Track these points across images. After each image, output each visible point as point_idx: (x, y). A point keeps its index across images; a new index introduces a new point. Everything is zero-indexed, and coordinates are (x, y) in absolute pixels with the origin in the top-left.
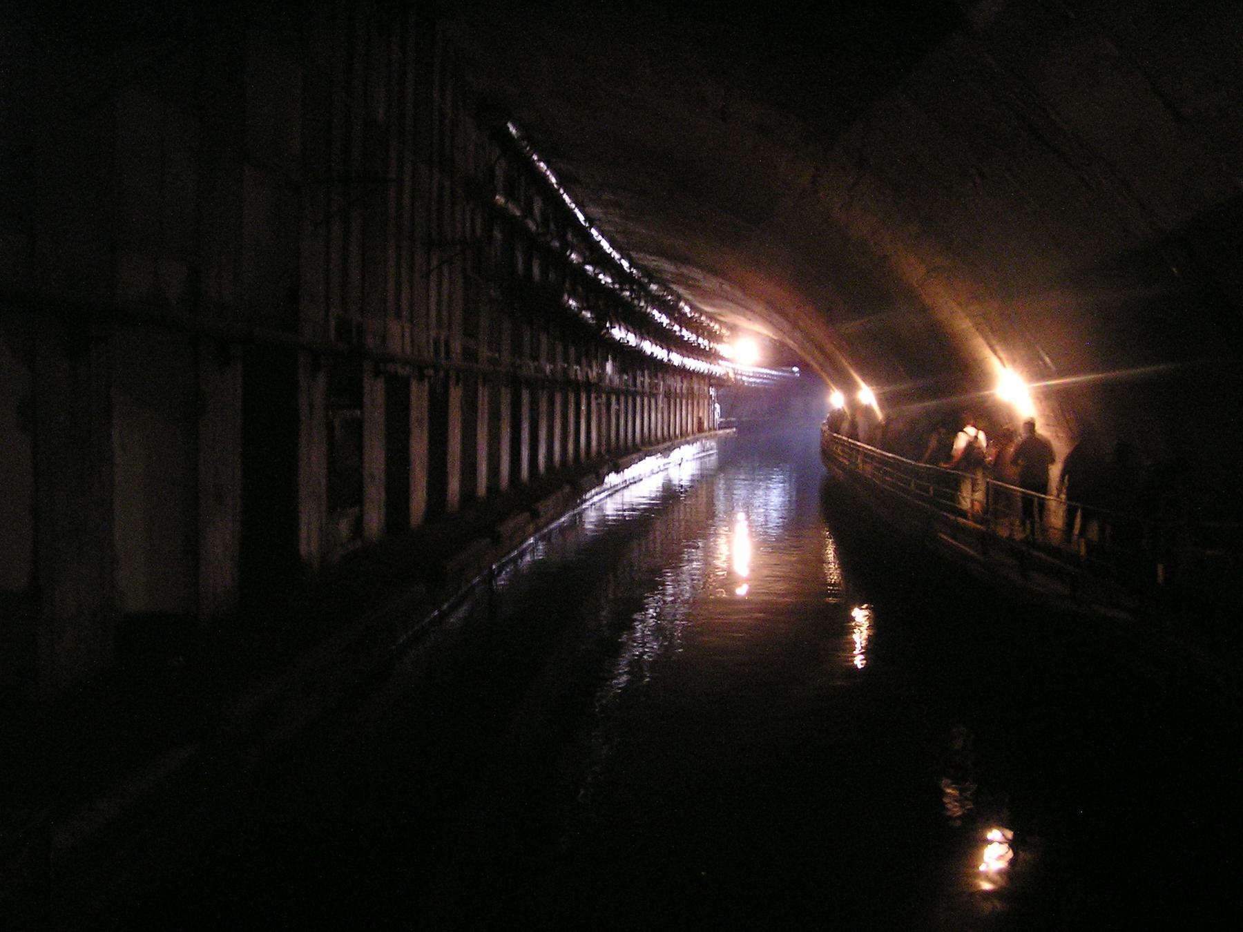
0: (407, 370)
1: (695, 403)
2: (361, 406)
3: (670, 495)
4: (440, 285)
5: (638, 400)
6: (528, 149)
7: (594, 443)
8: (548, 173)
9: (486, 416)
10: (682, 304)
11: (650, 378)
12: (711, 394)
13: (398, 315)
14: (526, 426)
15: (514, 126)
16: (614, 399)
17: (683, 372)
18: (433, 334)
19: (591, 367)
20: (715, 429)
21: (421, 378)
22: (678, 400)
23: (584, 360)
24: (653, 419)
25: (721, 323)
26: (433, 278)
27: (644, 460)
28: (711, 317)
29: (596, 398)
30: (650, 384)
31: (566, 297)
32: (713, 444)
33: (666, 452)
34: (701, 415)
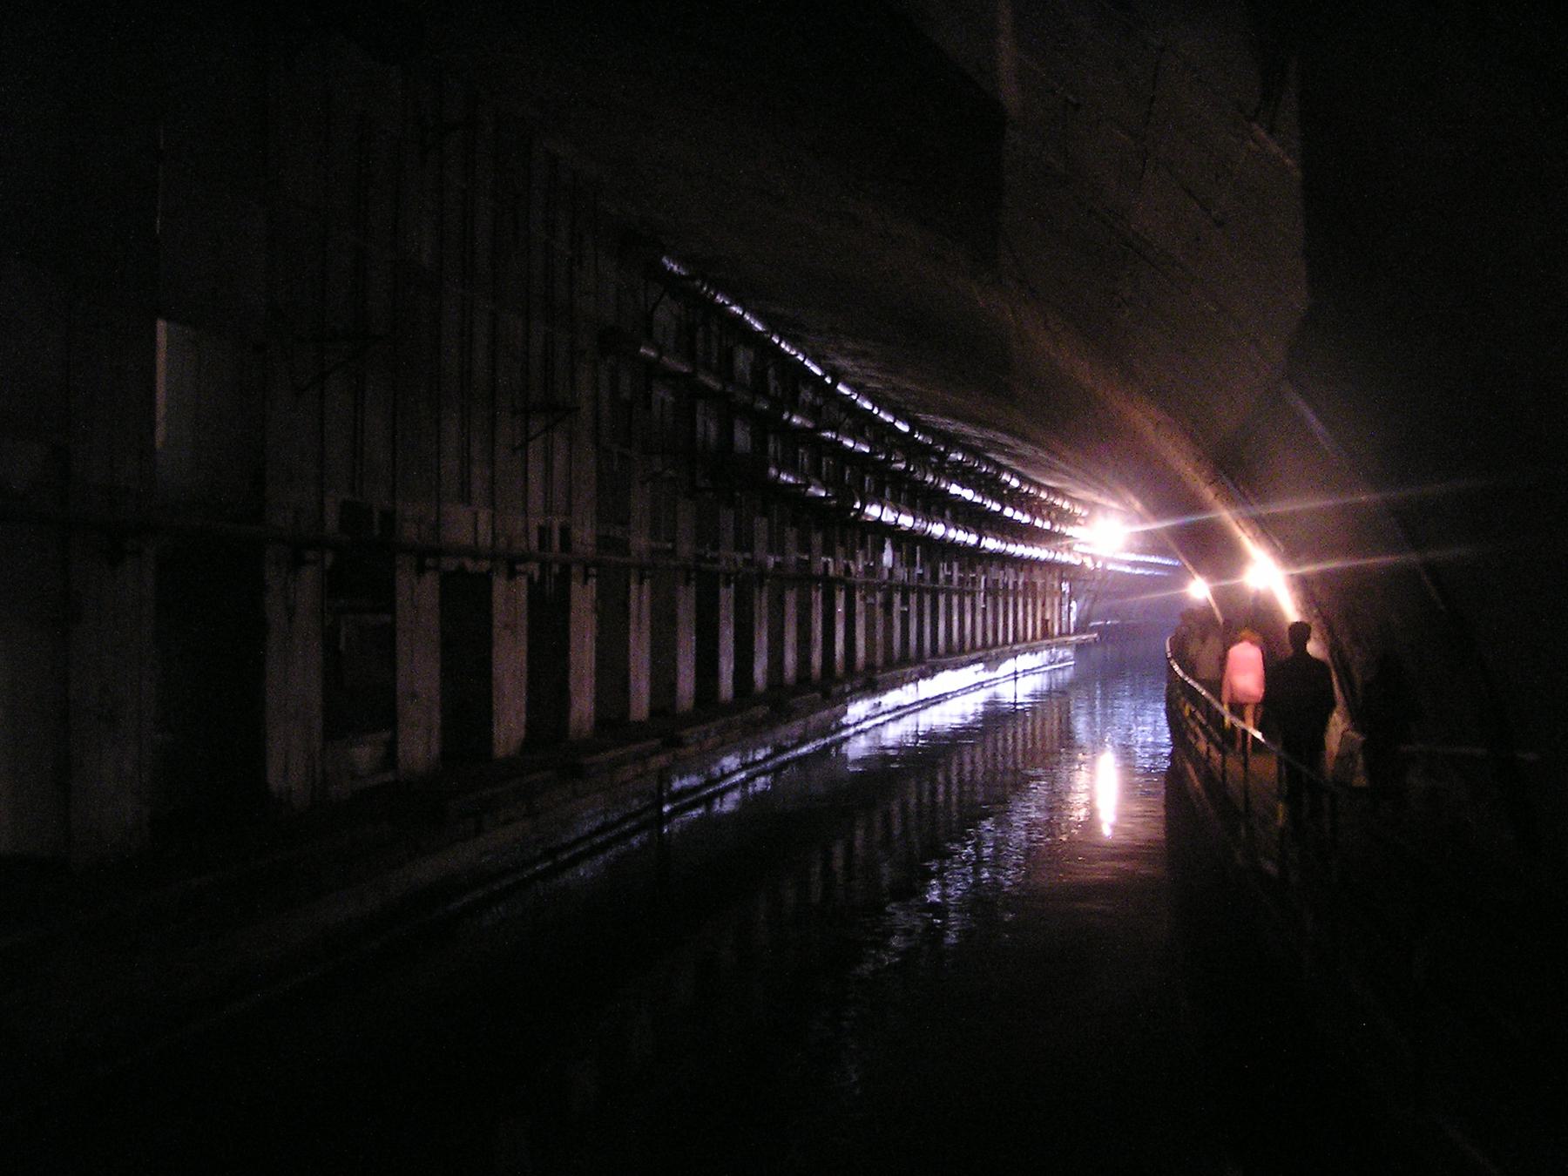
0: (485, 565)
1: (1039, 603)
2: (391, 608)
3: (996, 717)
4: (548, 461)
5: (942, 600)
6: (705, 289)
7: (861, 653)
8: (747, 317)
9: (646, 623)
10: (1005, 477)
11: (960, 570)
12: (1063, 590)
13: (465, 497)
14: (927, 621)
15: (675, 260)
16: (897, 598)
17: (1003, 559)
18: (535, 522)
19: (854, 558)
20: (1068, 634)
21: (512, 574)
22: (1011, 600)
23: (840, 551)
24: (971, 621)
25: (1072, 500)
26: (536, 446)
27: (928, 680)
28: (1053, 491)
29: (864, 598)
30: (961, 579)
31: (773, 472)
32: (1069, 653)
33: (992, 662)
34: (1048, 616)
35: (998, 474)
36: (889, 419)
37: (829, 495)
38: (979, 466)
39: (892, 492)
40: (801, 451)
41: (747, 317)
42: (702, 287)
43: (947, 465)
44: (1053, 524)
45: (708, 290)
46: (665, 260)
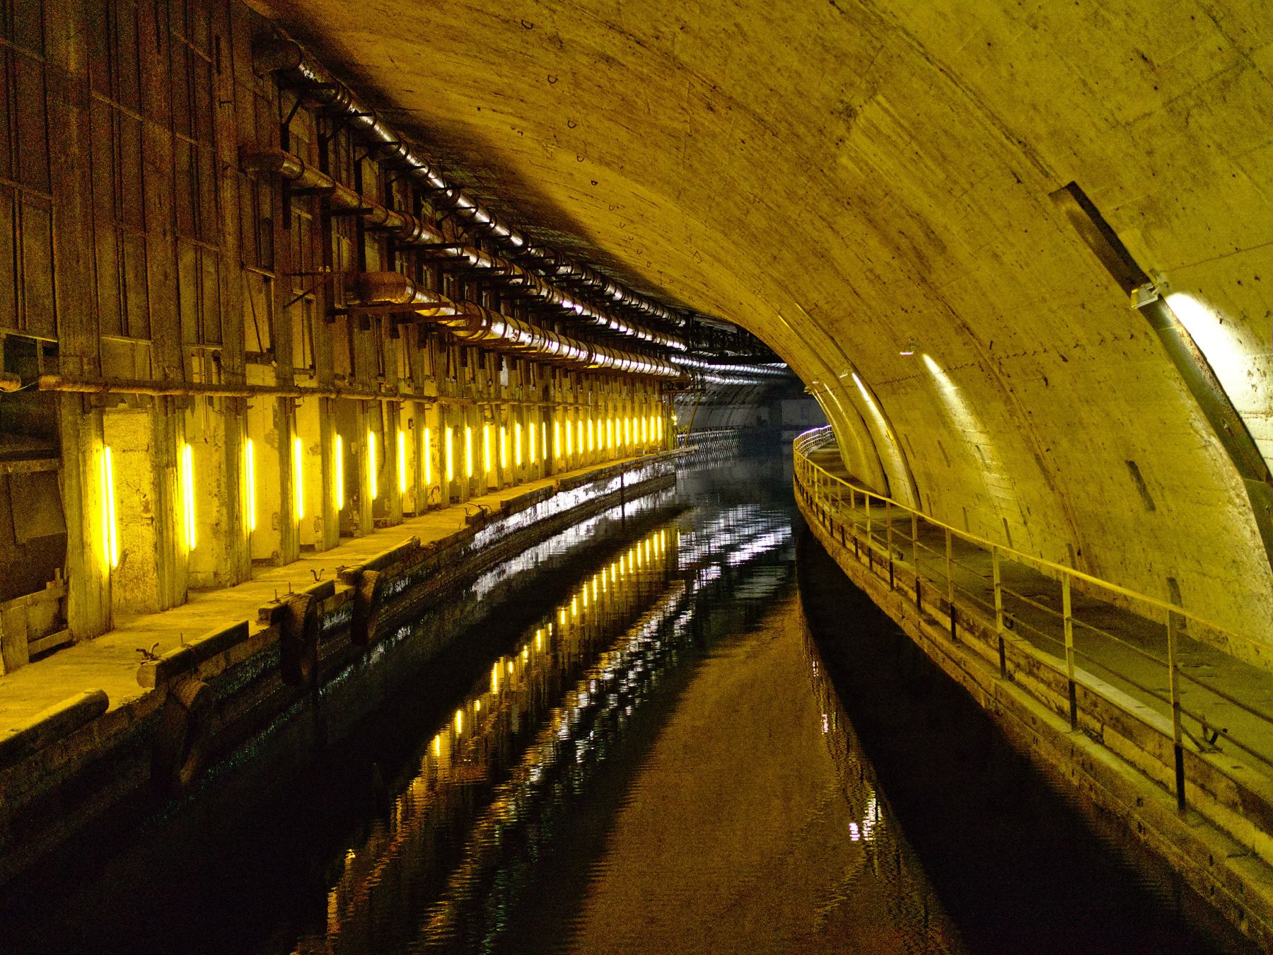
10: (610, 290)
35: (604, 286)
36: (504, 232)
37: (459, 313)
38: (586, 279)
39: (506, 308)
40: (425, 268)
41: (377, 128)
42: (336, 95)
43: (554, 279)
44: (654, 337)
45: (343, 98)
46: (302, 67)
